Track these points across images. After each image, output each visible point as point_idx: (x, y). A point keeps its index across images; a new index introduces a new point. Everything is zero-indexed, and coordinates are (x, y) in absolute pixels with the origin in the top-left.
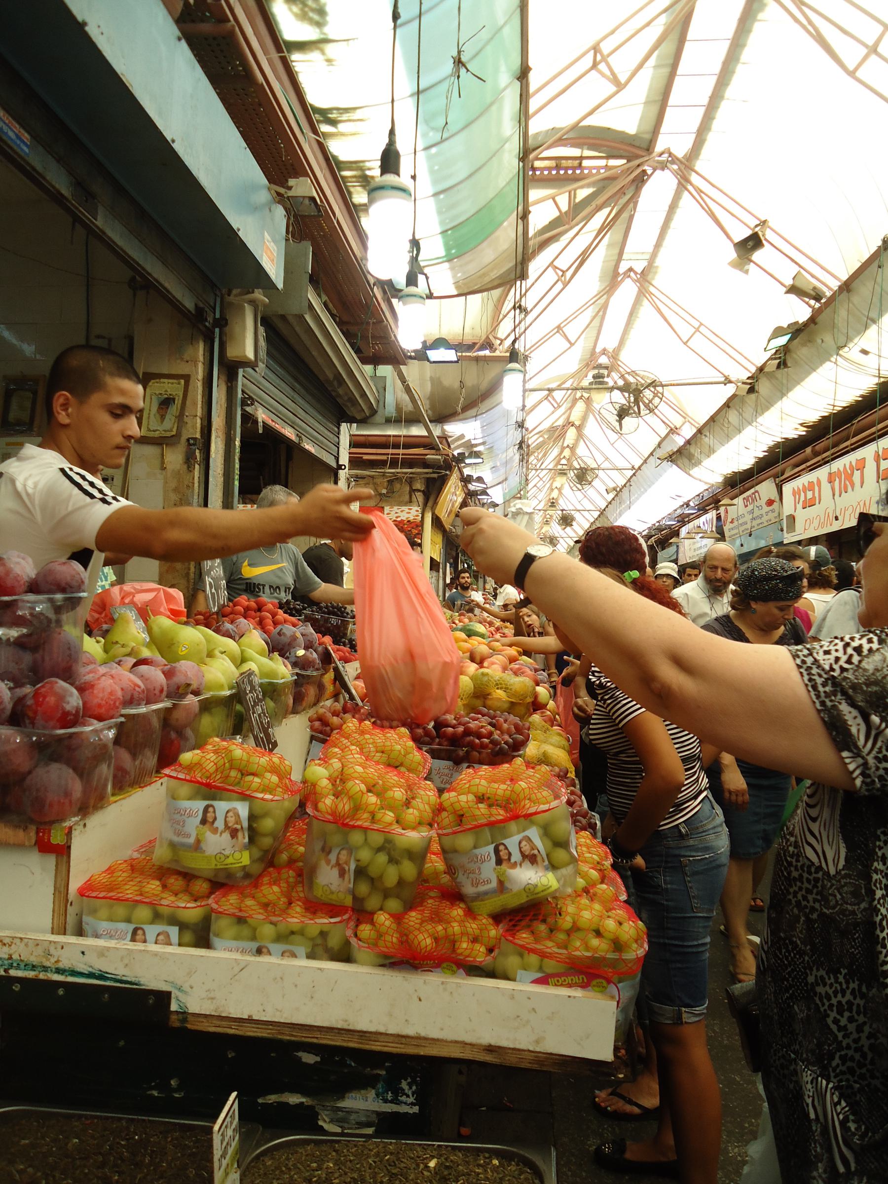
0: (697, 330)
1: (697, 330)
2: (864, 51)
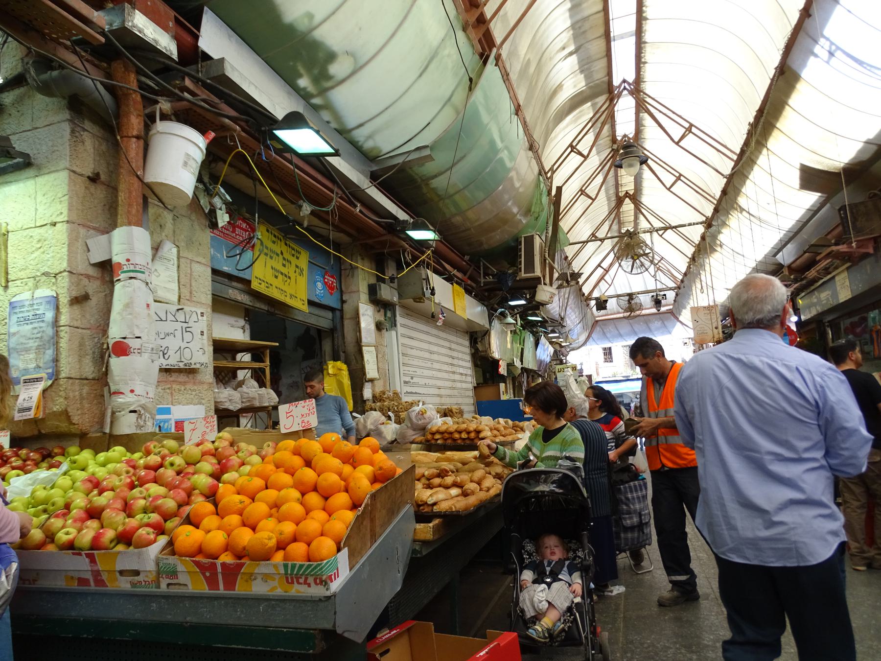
0: (678, 179)
1: (678, 179)
2: (675, 178)
